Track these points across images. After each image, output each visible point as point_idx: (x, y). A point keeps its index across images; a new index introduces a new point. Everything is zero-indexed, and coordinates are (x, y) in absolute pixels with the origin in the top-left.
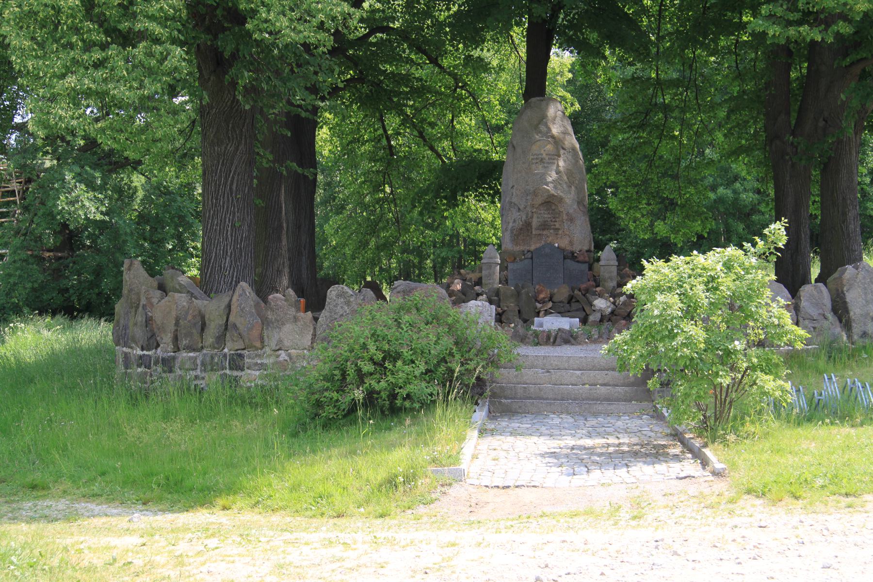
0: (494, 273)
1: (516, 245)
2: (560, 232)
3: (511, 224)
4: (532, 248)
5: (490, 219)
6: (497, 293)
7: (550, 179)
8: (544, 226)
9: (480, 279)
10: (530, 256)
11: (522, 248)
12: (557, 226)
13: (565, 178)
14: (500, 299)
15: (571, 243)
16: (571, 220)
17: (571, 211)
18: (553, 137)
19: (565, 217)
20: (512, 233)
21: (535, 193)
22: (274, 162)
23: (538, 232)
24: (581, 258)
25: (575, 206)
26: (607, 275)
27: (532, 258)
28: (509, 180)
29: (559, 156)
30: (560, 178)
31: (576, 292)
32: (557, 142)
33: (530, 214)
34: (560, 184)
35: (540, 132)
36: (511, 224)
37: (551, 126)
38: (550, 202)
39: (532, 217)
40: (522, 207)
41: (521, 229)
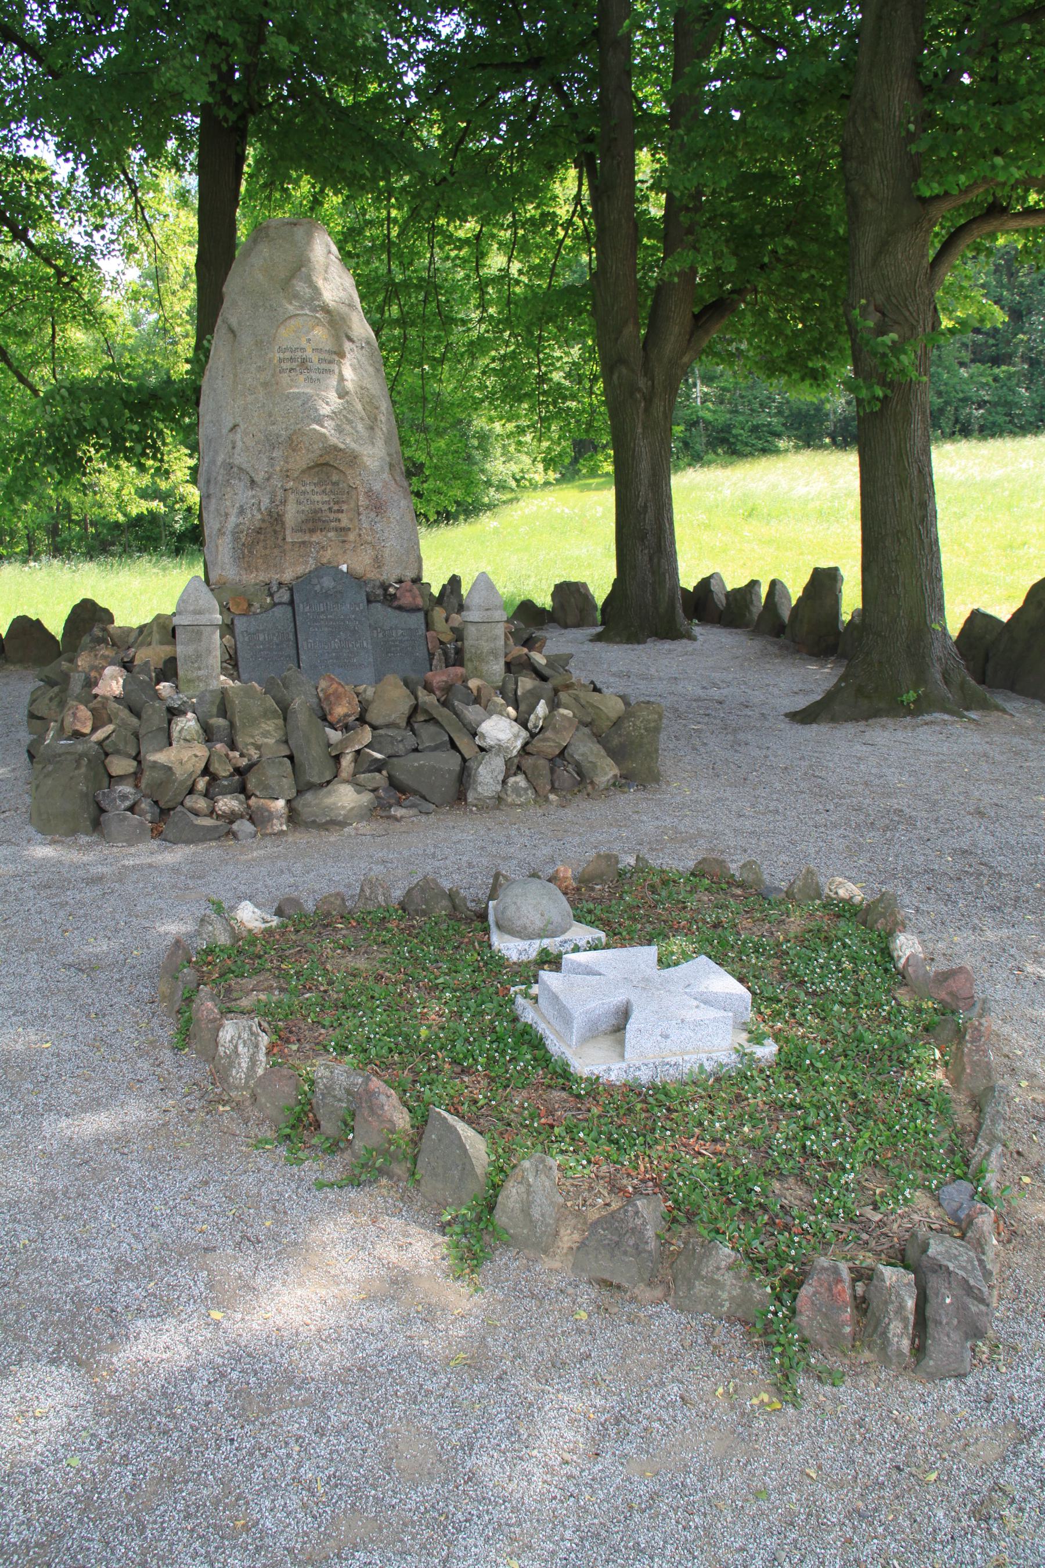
0: (209, 652)
1: (249, 568)
2: (352, 537)
3: (233, 520)
4: (288, 576)
5: (115, 485)
6: (223, 705)
7: (325, 410)
8: (314, 523)
9: (172, 661)
10: (286, 598)
11: (263, 577)
12: (345, 523)
13: (359, 407)
14: (232, 725)
15: (378, 562)
16: (378, 507)
17: (377, 486)
18: (326, 309)
19: (363, 501)
20: (236, 538)
21: (292, 443)
22: (822, 402)
23: (299, 537)
24: (406, 600)
25: (386, 476)
26: (485, 646)
27: (291, 603)
28: (220, 405)
29: (342, 355)
30: (349, 407)
31: (423, 696)
32: (336, 322)
33: (280, 493)
34: (350, 422)
35: (296, 296)
36: (233, 520)
37: (320, 283)
38: (329, 466)
39: (284, 502)
40: (259, 478)
41: (259, 531)
